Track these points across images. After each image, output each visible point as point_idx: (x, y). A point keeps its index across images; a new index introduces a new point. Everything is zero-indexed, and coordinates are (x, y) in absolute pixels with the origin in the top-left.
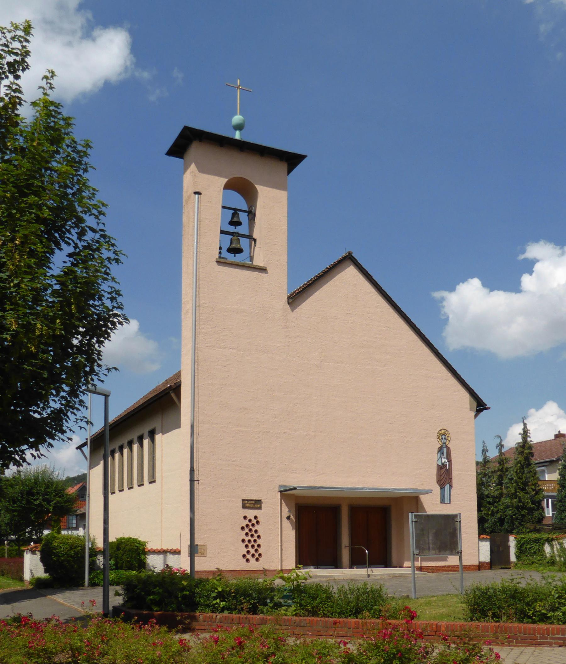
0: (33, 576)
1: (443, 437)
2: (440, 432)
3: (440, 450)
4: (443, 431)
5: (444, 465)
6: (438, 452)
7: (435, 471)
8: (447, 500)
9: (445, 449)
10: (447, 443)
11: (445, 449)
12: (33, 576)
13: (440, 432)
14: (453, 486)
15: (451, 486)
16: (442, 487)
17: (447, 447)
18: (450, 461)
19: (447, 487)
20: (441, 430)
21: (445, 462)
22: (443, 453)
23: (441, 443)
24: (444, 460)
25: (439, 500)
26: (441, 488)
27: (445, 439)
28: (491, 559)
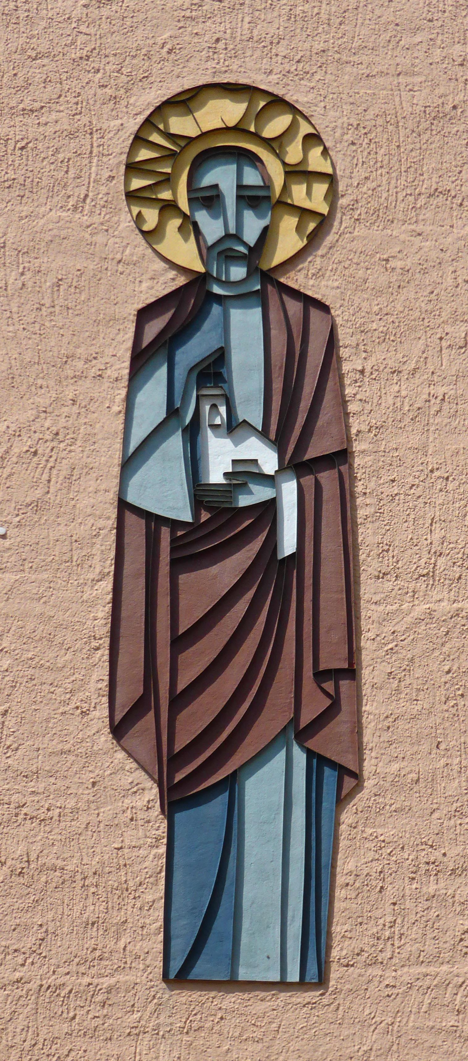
0: (137, 769)
1: (222, 177)
2: (181, 125)
3: (172, 327)
4: (223, 112)
5: (222, 518)
6: (141, 360)
7: (85, 599)
8: (264, 941)
9: (245, 333)
10: (288, 242)
11: (245, 333)
12: (137, 769)
13: (181, 125)
14: (375, 766)
15: (333, 778)
16: (194, 782)
17: (268, 285)
18: (320, 462)
19: (269, 791)
20: (186, 101)
21: (244, 474)
22: (213, 371)
23: (187, 254)
24: (220, 457)
25: (141, 935)
26: (176, 800)
27: (251, 199)
28: (297, 549)
